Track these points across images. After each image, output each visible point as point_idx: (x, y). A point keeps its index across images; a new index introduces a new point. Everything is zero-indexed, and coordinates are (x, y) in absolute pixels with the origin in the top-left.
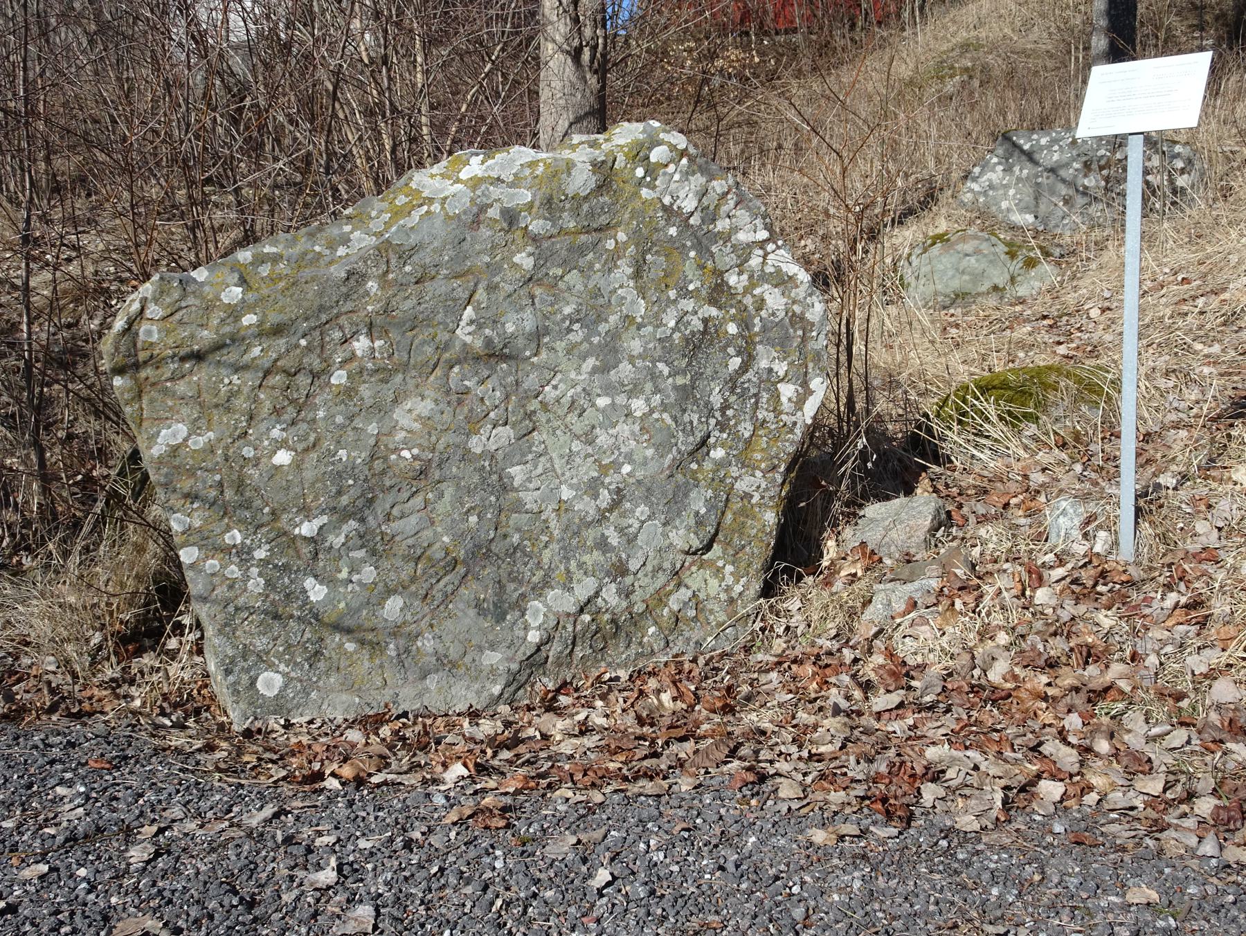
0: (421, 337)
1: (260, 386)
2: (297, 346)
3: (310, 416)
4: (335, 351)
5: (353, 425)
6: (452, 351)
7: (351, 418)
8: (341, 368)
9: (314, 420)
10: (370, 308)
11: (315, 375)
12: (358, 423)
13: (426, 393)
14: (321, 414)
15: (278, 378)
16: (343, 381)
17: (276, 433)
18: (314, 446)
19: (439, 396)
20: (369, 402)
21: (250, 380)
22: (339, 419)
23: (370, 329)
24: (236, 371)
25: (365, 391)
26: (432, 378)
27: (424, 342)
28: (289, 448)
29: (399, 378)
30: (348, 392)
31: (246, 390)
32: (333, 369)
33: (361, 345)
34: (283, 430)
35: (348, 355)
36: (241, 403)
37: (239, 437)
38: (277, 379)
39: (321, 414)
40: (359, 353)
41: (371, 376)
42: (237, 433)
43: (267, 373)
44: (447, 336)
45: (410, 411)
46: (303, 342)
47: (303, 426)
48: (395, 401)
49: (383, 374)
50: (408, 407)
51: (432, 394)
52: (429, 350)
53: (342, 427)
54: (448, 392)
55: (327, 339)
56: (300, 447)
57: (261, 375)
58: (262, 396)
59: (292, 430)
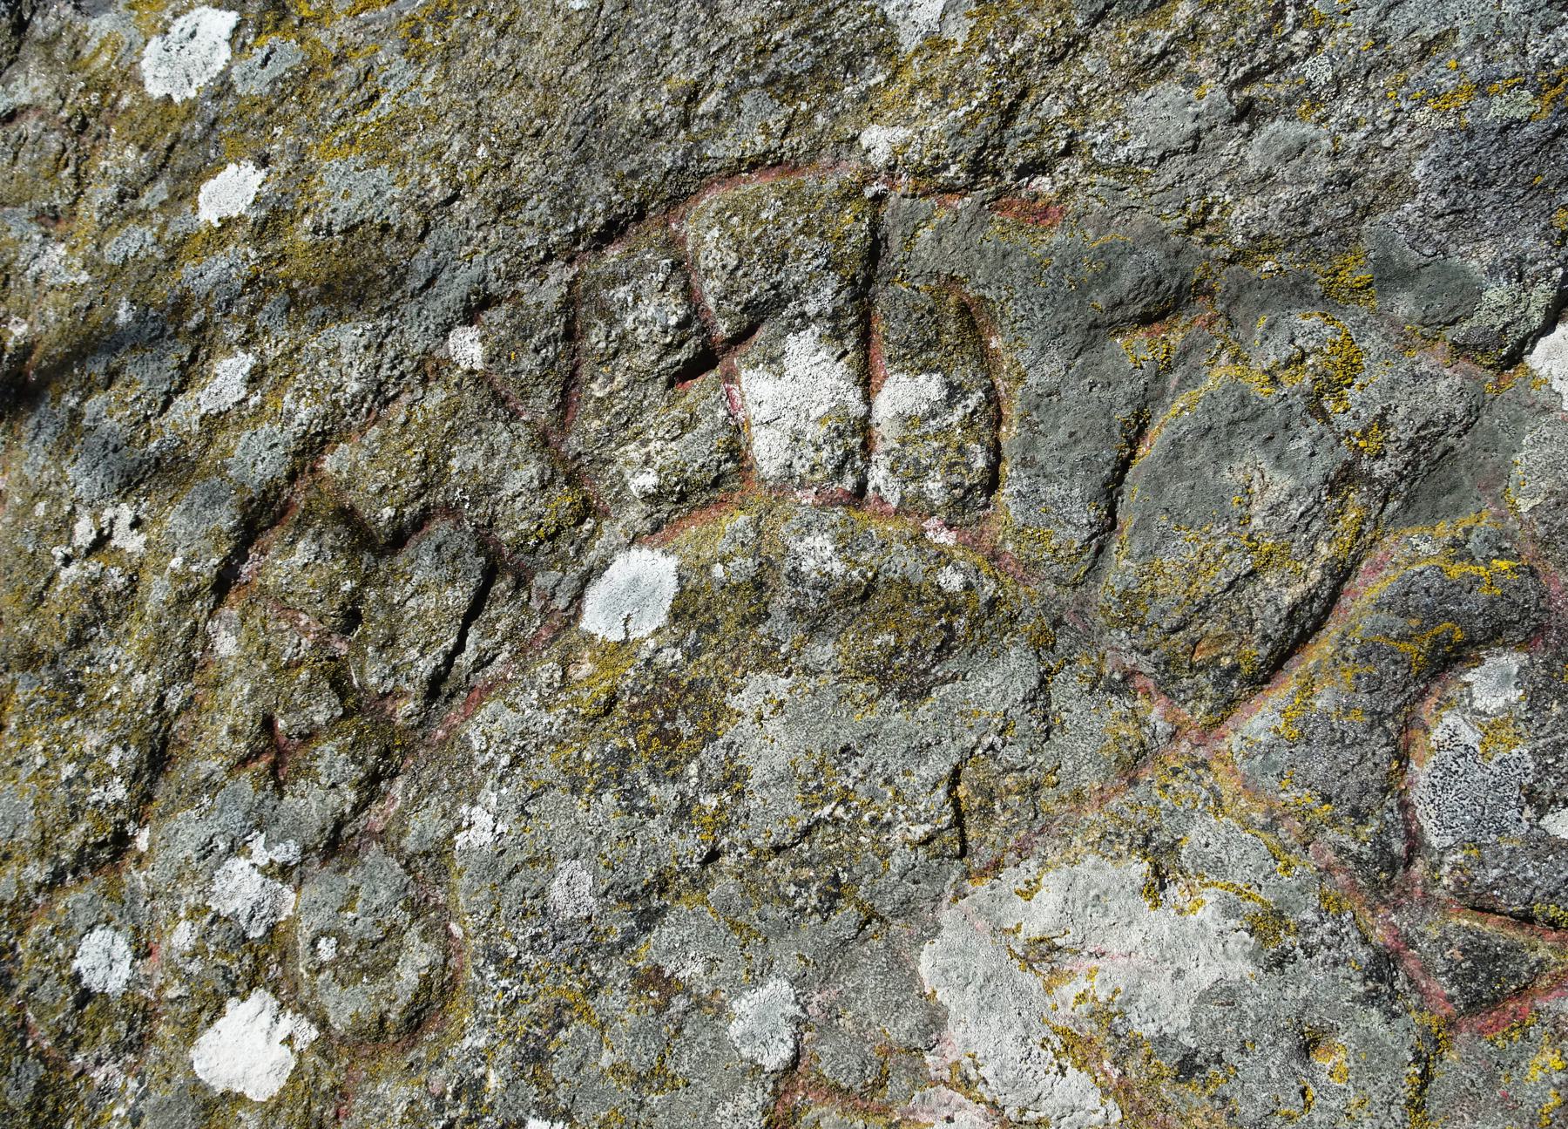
0: (1219, 375)
1: (224, 583)
2: (430, 369)
3: (424, 825)
4: (627, 424)
5: (652, 948)
6: (1480, 521)
7: (645, 903)
8: (655, 532)
9: (438, 855)
10: (879, 140)
11: (497, 568)
12: (682, 946)
13: (1199, 835)
14: (481, 828)
15: (303, 551)
16: (650, 622)
17: (241, 886)
18: (415, 1022)
19: (1292, 882)
20: (772, 811)
21: (170, 541)
22: (573, 890)
23: (861, 292)
24: (129, 484)
25: (770, 725)
26: (1261, 719)
27: (1240, 421)
28: (290, 999)
29: (995, 684)
30: (663, 716)
31: (157, 592)
32: (613, 531)
33: (789, 393)
34: (284, 872)
35: (696, 452)
36: (125, 669)
37: (85, 861)
38: (293, 561)
39: (481, 828)
40: (767, 451)
41: (816, 627)
42: (73, 838)
43: (260, 517)
44: (1445, 386)
45: (1044, 952)
46: (468, 348)
47: (378, 881)
48: (955, 845)
49: (910, 636)
50: (1039, 916)
51: (1246, 857)
52: (1270, 484)
53: (587, 948)
54: (1389, 869)
55: (596, 338)
56: (348, 1006)
57: (226, 518)
58: (226, 644)
59: (323, 887)
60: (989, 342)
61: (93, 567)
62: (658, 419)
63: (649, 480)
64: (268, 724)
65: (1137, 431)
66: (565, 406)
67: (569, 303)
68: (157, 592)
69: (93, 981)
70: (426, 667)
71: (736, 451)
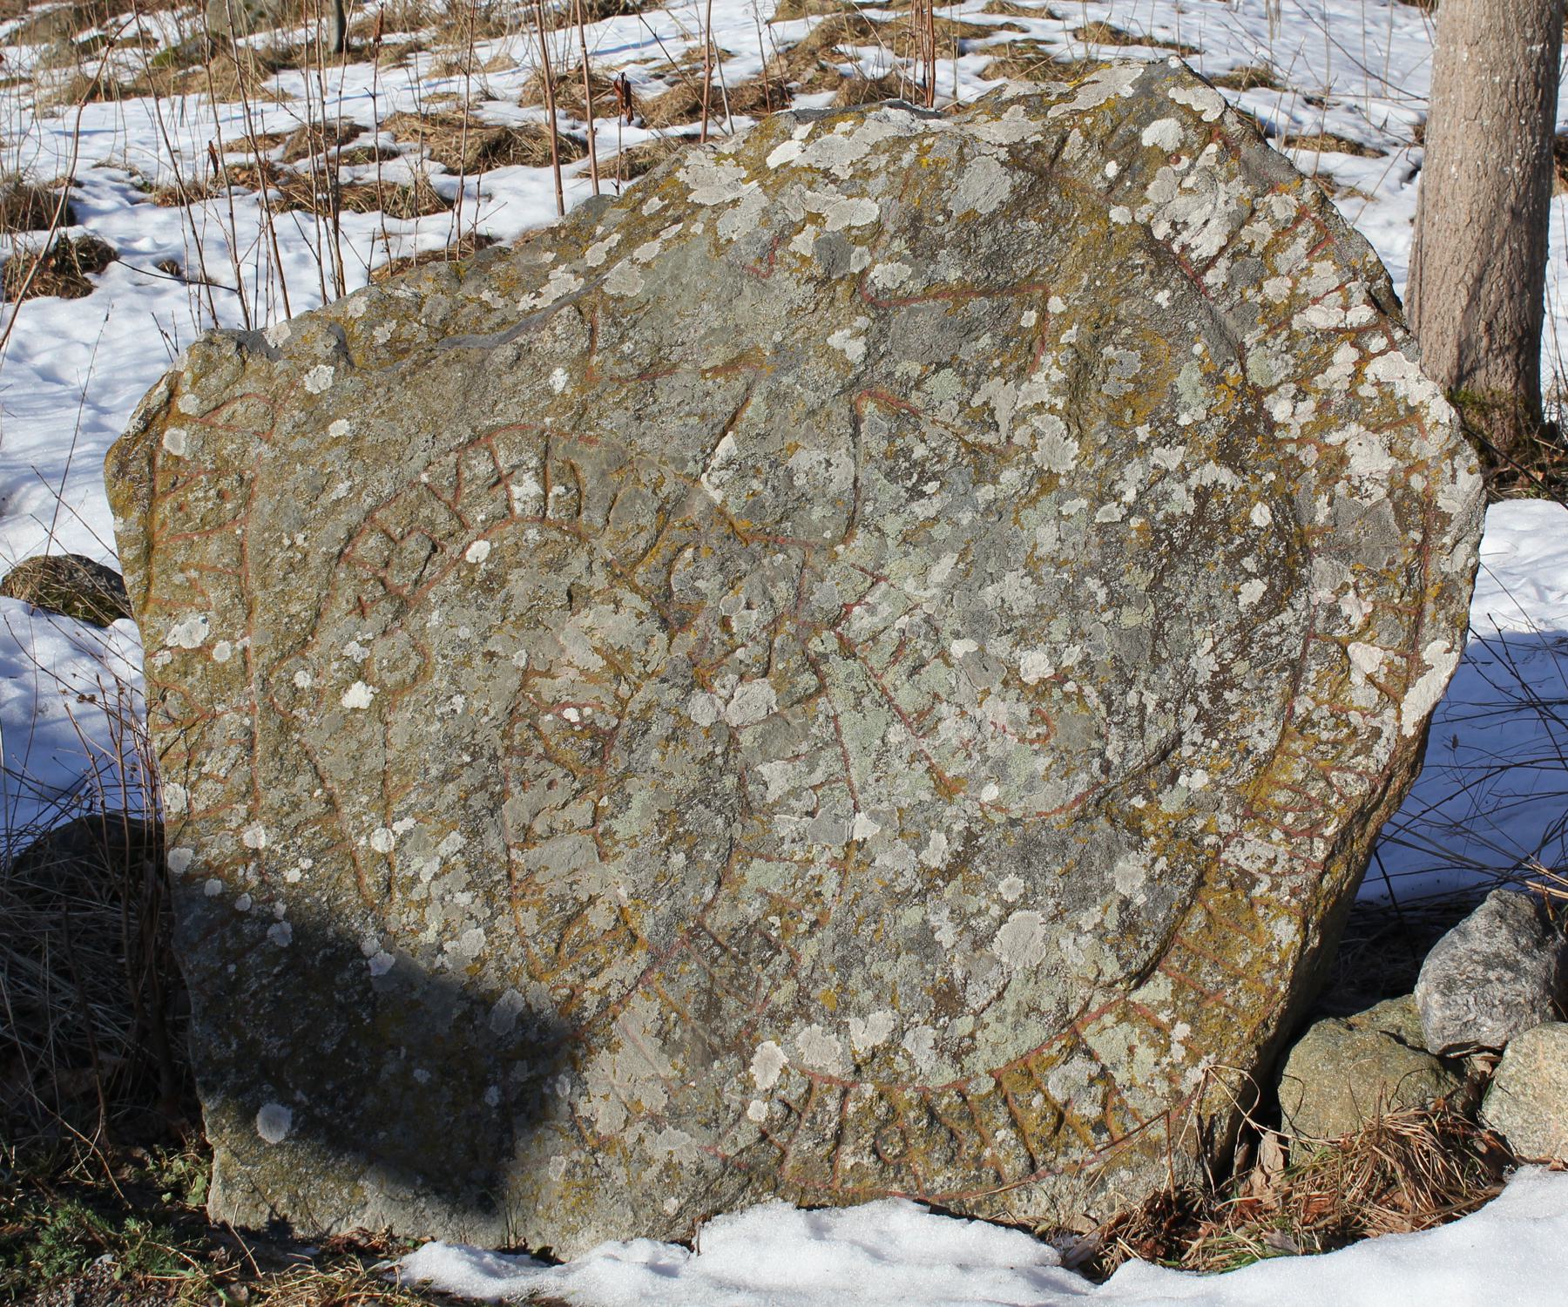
31: (315, 560)
32: (472, 533)
35: (498, 508)
39: (435, 618)
60: (1246, 183)
61: (290, 554)
62: (486, 499)
63: (483, 517)
64: (359, 599)
65: (283, 287)
66: (456, 496)
67: (457, 465)
68: (315, 560)
69: (299, 685)
70: (414, 576)
71: (509, 508)
